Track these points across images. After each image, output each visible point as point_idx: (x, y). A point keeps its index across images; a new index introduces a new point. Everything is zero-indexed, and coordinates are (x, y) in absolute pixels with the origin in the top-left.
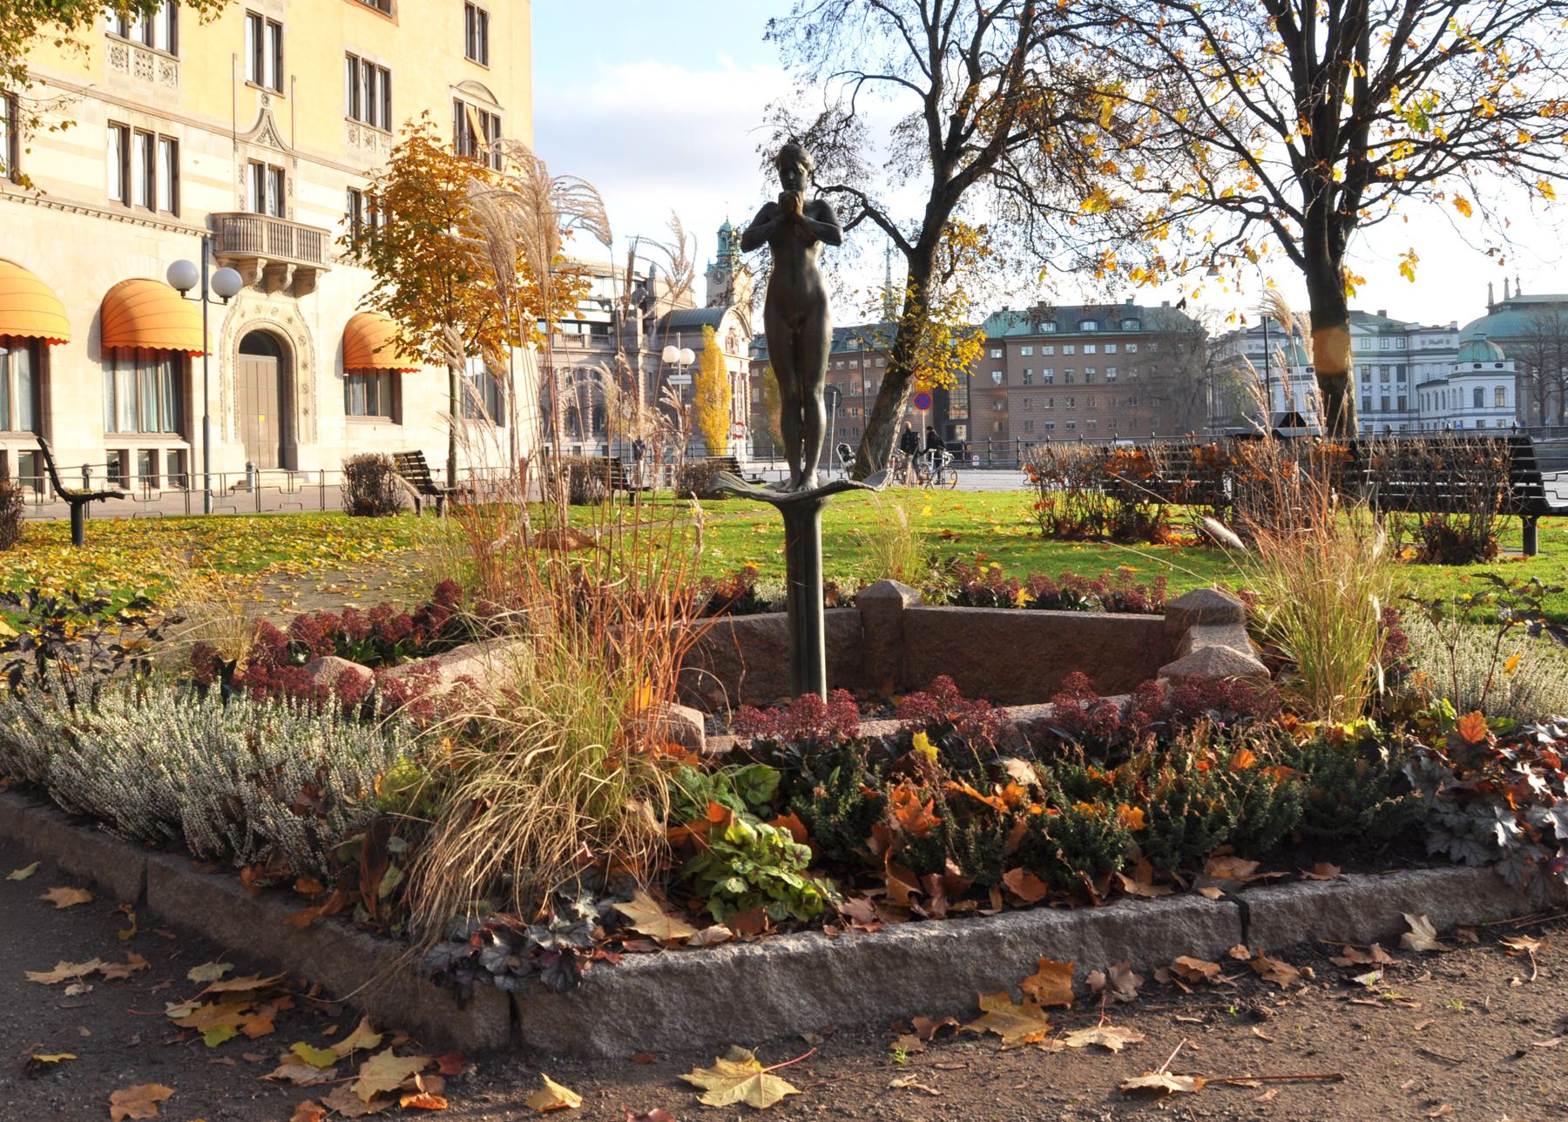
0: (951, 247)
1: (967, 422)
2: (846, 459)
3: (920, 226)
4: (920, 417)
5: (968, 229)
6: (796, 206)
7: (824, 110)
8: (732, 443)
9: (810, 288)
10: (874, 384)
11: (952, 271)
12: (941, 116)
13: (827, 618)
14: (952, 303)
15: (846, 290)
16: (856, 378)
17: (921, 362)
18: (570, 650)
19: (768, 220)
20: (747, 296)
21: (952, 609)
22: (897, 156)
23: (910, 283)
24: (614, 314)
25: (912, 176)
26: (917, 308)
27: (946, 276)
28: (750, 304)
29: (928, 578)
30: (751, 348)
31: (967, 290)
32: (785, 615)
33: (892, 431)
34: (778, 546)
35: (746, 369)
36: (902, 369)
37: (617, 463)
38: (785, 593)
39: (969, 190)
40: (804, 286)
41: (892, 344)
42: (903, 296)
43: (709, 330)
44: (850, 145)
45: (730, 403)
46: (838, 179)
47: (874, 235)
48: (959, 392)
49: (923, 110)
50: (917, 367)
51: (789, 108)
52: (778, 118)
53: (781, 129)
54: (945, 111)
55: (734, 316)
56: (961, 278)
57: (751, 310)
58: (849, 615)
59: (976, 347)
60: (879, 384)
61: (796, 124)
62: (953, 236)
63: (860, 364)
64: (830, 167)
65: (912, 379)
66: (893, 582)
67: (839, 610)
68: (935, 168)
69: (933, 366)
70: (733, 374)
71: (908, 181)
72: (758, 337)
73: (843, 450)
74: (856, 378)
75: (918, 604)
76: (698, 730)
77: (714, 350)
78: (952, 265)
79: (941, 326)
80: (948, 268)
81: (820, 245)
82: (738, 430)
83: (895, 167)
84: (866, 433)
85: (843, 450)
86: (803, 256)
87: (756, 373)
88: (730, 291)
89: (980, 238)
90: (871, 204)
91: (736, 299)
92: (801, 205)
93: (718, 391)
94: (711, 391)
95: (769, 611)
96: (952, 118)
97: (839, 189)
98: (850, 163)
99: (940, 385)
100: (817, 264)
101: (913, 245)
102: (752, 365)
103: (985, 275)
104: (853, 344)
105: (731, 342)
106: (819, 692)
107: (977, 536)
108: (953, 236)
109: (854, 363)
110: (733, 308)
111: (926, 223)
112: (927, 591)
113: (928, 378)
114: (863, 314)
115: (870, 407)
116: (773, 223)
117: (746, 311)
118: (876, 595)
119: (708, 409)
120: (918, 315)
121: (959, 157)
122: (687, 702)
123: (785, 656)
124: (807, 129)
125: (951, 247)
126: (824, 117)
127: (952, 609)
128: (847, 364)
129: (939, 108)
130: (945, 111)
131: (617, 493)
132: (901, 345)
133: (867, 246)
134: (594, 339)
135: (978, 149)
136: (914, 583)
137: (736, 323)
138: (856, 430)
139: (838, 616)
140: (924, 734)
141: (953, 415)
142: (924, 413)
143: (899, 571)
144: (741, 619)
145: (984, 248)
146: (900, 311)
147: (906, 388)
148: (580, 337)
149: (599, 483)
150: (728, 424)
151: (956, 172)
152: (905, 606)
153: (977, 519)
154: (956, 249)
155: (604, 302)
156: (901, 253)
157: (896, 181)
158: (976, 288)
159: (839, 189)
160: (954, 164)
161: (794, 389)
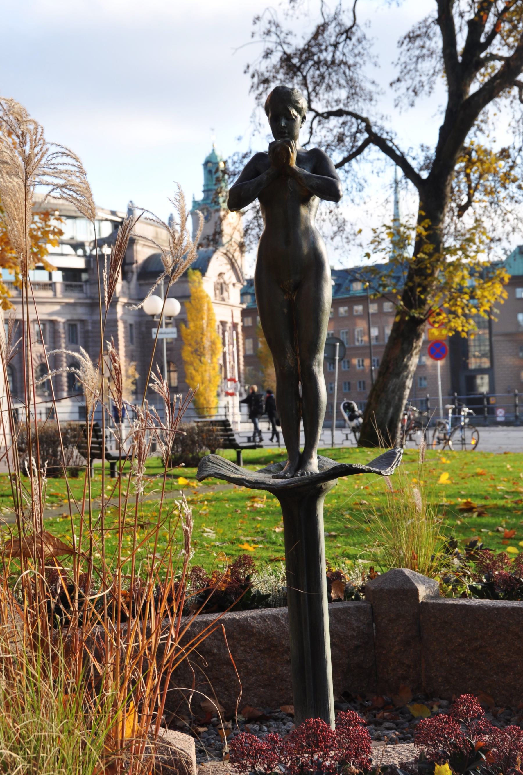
0: (468, 176)
1: (489, 371)
2: (352, 418)
3: (432, 153)
4: (435, 367)
5: (487, 153)
6: (288, 157)
7: (321, 21)
8: (224, 401)
9: (305, 249)
10: (382, 331)
11: (469, 203)
12: (457, 20)
13: (332, 613)
14: (470, 240)
15: (348, 228)
16: (361, 325)
17: (436, 309)
18: (45, 676)
19: (258, 173)
20: (237, 238)
21: (475, 602)
22: (406, 71)
23: (421, 219)
24: (89, 259)
25: (423, 95)
26: (429, 247)
27: (462, 209)
28: (242, 246)
29: (447, 566)
30: (243, 294)
31: (487, 224)
32: (285, 610)
33: (403, 387)
34: (276, 522)
35: (238, 319)
36: (413, 318)
37: (97, 431)
38: (283, 584)
39: (490, 107)
40: (300, 247)
41: (402, 287)
42: (413, 234)
43: (196, 276)
44: (351, 61)
45: (220, 356)
46: (338, 101)
47: (380, 165)
48: (479, 339)
49: (436, 15)
50: (430, 312)
51: (280, 19)
52: (268, 33)
53: (272, 46)
54: (461, 15)
55: (224, 260)
56: (479, 211)
57: (242, 252)
58: (358, 608)
59: (498, 289)
60: (388, 331)
61: (290, 39)
62: (470, 163)
63: (366, 309)
64: (329, 88)
65: (426, 326)
66: (407, 571)
67: (347, 604)
68: (450, 84)
69: (450, 312)
70: (223, 323)
71: (417, 100)
72: (249, 281)
73: (349, 408)
74: (361, 325)
75: (436, 597)
76: (188, 757)
77: (200, 299)
78: (470, 196)
79: (457, 266)
80: (465, 199)
81: (316, 200)
82: (230, 386)
83: (403, 85)
84: (374, 389)
85: (349, 408)
86: (297, 214)
87: (249, 321)
88: (219, 233)
89: (502, 163)
90: (375, 129)
91: (225, 239)
92: (294, 156)
93: (207, 343)
94: (199, 343)
95: (268, 606)
96: (470, 23)
97: (339, 113)
98: (352, 84)
99: (458, 333)
100: (314, 224)
101: (425, 175)
102: (244, 313)
103: (507, 205)
104: (357, 287)
105: (221, 287)
106: (327, 718)
107: (504, 508)
108: (470, 163)
109: (359, 308)
110: (222, 250)
111: (439, 149)
112: (446, 580)
113: (442, 325)
114: (368, 255)
115: (379, 357)
116: (263, 176)
117: (237, 254)
118: (388, 586)
119: (196, 363)
120: (430, 255)
121: (477, 69)
122: (173, 726)
123: (286, 657)
124: (301, 44)
125: (468, 176)
126: (321, 29)
127: (475, 602)
128: (351, 310)
129: (455, 12)
130: (461, 15)
131: (97, 462)
132: (412, 290)
133: (372, 179)
134: (68, 287)
135: (500, 58)
136: (430, 572)
137: (226, 268)
138: (362, 384)
139: (346, 610)
140: (447, 766)
141: (473, 364)
142: (440, 363)
143: (414, 558)
144: (237, 615)
145: (507, 175)
146: (409, 252)
147: (418, 337)
148: (50, 286)
149: (76, 452)
150: (218, 380)
151: (474, 88)
152: (421, 599)
153: (502, 487)
154: (474, 177)
155: (77, 246)
156: (411, 184)
157: (405, 102)
158: (497, 221)
159: (339, 113)
160: (471, 77)
161: (290, 361)
